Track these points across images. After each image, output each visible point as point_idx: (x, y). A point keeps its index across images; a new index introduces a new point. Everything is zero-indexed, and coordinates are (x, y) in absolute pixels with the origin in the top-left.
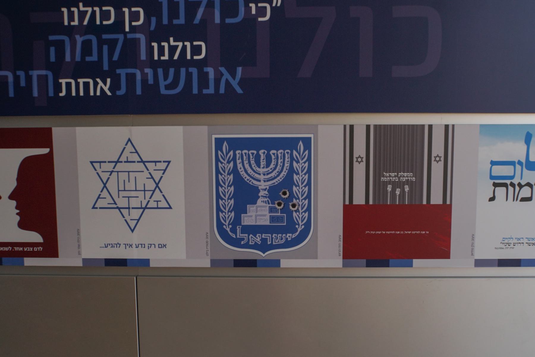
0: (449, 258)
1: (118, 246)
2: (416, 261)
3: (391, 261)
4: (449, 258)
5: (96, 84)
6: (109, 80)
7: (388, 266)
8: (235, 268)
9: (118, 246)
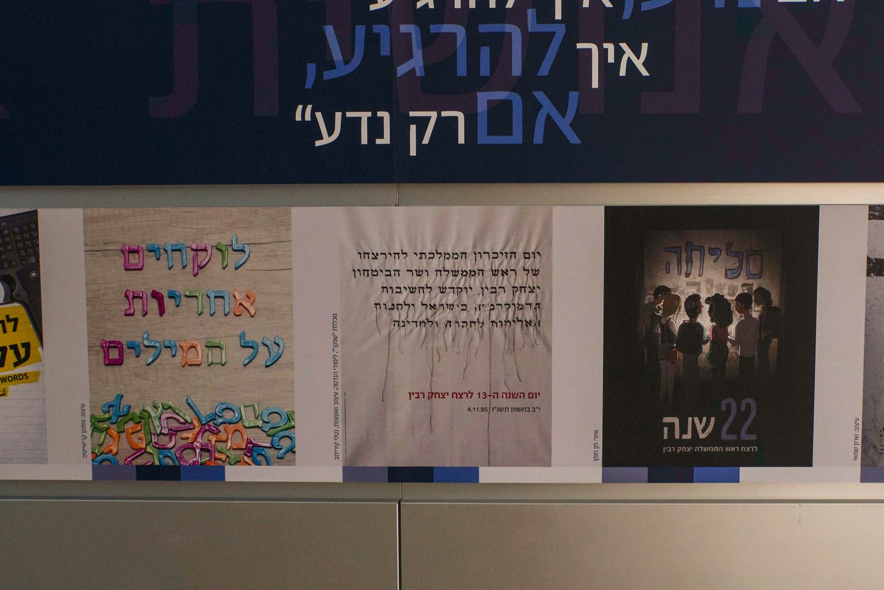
0: (810, 465)
1: (470, 395)
2: (745, 472)
3: (697, 471)
4: (810, 465)
5: (619, 53)
6: (645, 47)
7: (689, 479)
8: (391, 484)
9: (470, 395)
